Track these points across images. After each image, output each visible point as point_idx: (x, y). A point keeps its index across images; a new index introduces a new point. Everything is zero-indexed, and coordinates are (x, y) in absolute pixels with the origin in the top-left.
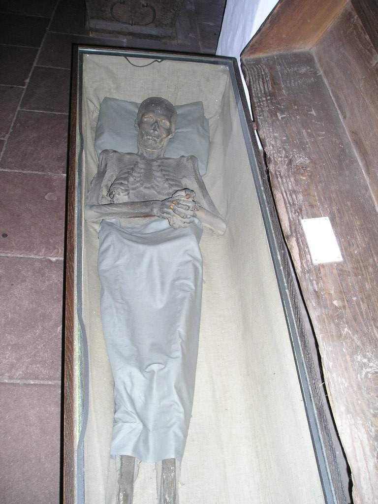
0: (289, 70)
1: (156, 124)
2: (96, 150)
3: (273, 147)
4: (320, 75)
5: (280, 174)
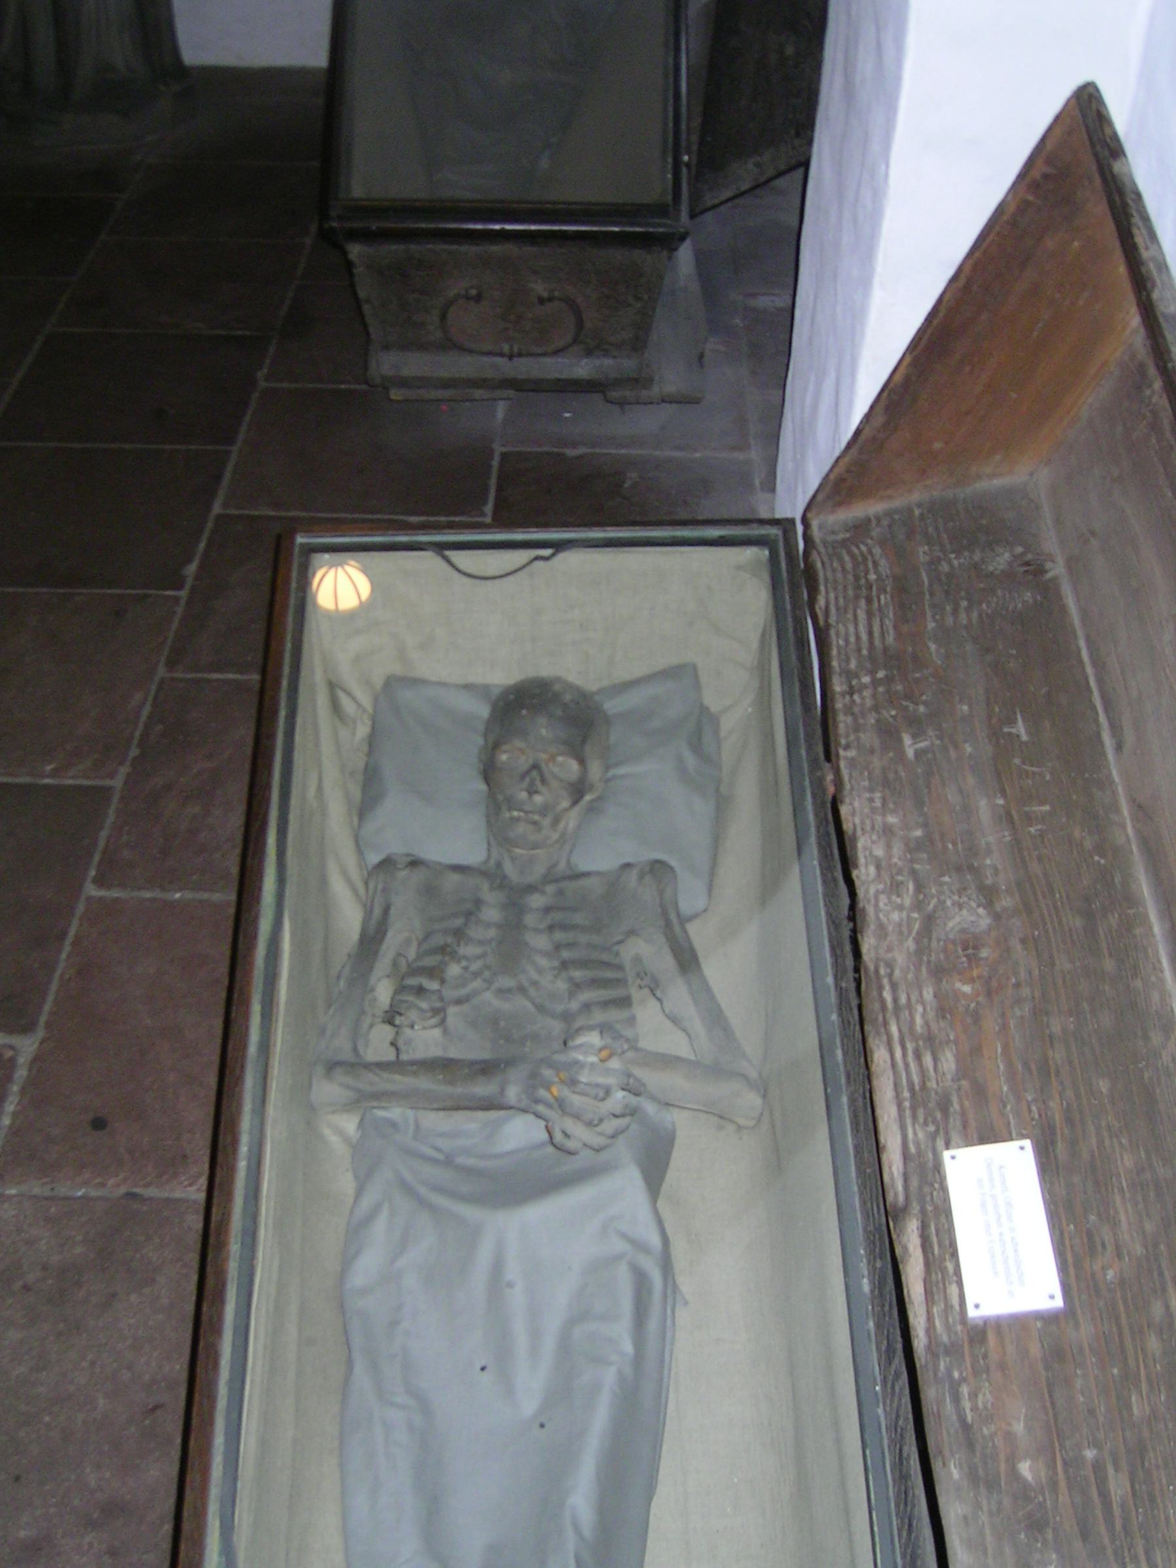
0: (956, 563)
1: (534, 773)
2: (360, 851)
3: (878, 867)
4: (1055, 579)
5: (890, 975)
